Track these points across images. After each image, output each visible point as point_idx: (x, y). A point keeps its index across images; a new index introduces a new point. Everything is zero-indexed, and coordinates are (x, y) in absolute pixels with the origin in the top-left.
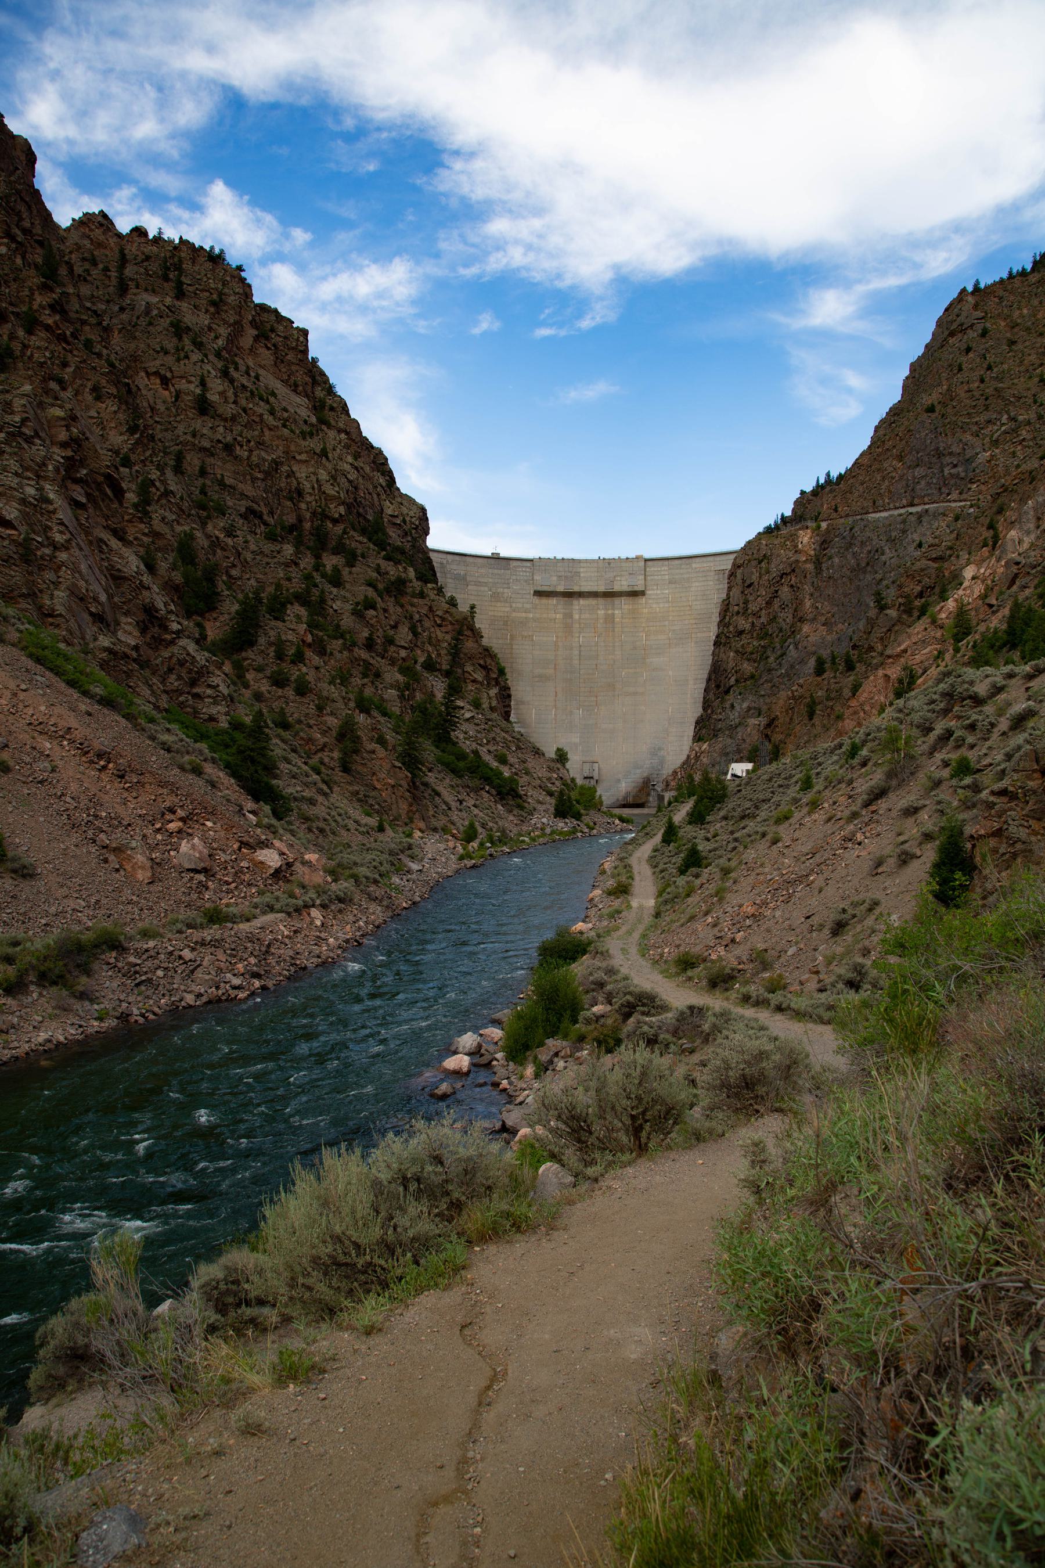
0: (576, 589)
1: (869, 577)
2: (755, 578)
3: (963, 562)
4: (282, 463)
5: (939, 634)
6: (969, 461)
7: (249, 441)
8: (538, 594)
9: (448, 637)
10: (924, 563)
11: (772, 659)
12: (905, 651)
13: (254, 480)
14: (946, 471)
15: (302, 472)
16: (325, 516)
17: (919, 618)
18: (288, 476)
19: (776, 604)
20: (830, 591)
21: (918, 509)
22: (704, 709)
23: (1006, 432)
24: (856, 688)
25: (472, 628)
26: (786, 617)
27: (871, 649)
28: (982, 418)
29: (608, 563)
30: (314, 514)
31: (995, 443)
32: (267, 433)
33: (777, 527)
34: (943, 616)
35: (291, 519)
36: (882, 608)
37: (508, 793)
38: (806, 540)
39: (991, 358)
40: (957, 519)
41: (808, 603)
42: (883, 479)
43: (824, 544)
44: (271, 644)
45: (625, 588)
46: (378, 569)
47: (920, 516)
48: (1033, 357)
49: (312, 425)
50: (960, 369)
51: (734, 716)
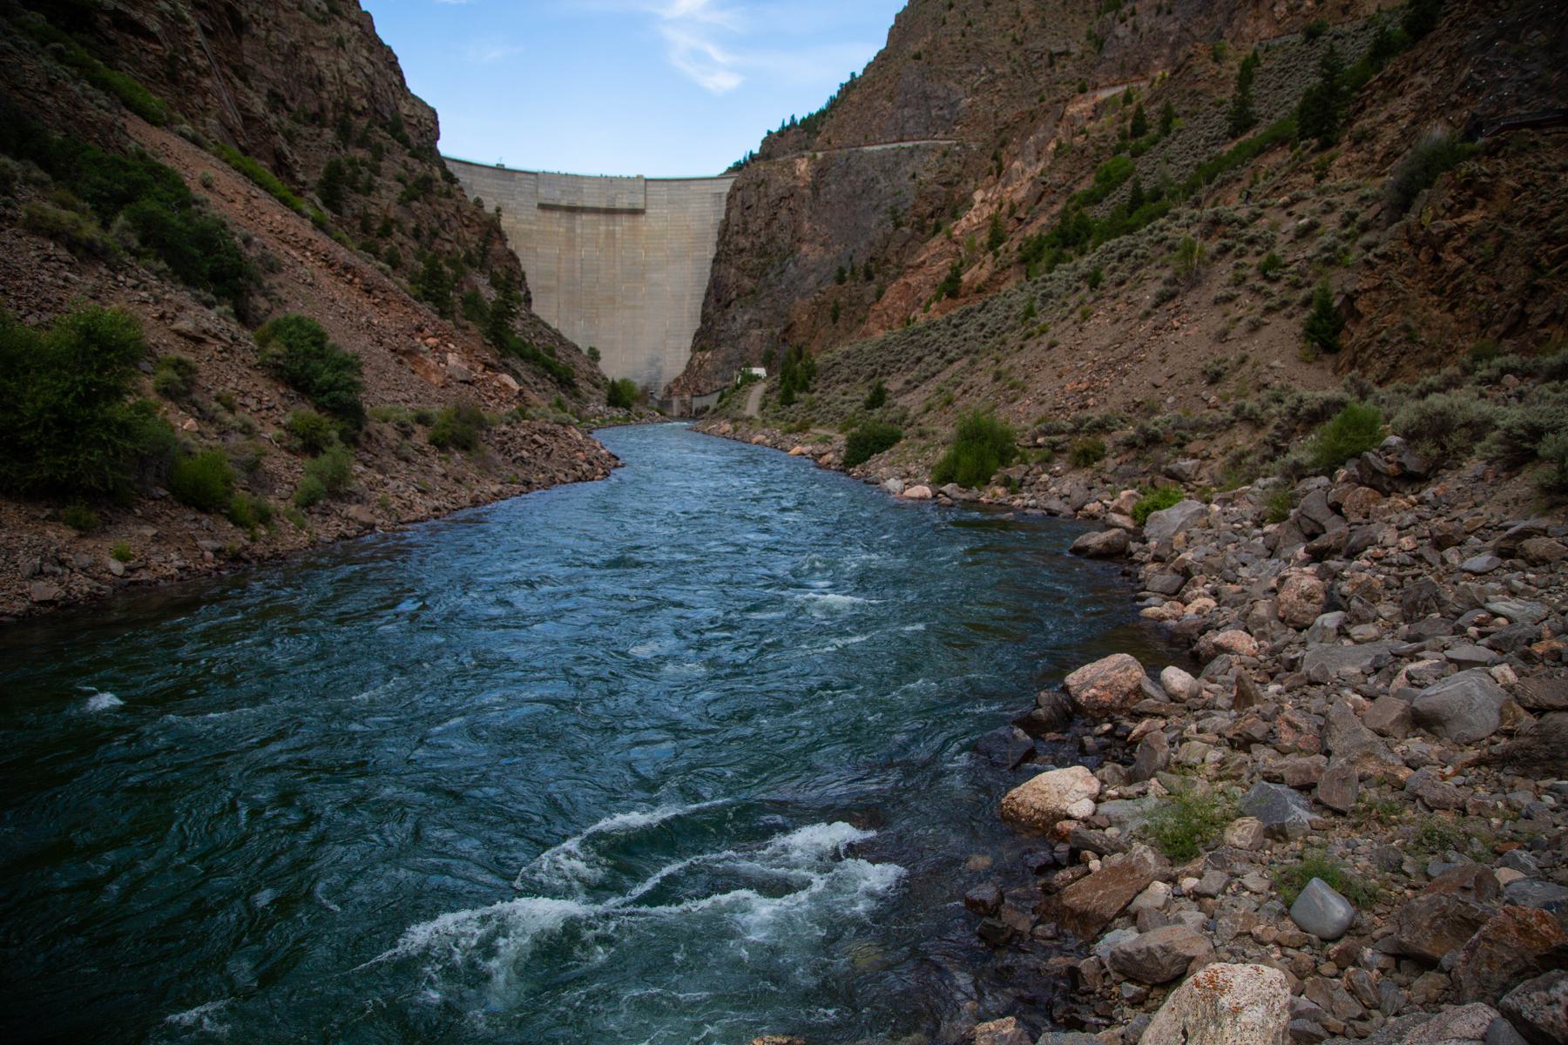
0: (579, 204)
1: (865, 204)
2: (754, 200)
3: (971, 187)
4: (301, 48)
5: (953, 248)
6: (954, 105)
7: (266, 20)
8: (543, 207)
9: (476, 238)
10: (936, 186)
11: (771, 276)
12: (924, 262)
13: (274, 62)
14: (934, 113)
15: (321, 60)
16: (348, 108)
17: (934, 234)
18: (308, 62)
19: (775, 225)
20: (827, 215)
21: (910, 144)
22: (704, 321)
23: (984, 83)
24: (879, 295)
25: (499, 231)
26: (785, 238)
27: (887, 261)
28: (964, 68)
29: (611, 180)
30: (336, 104)
31: (976, 91)
32: (282, 14)
33: (746, 163)
34: (957, 232)
35: (313, 107)
36: (898, 225)
37: (565, 382)
38: (803, 167)
39: (970, 15)
40: (945, 155)
41: (807, 225)
42: (874, 116)
43: (821, 171)
44: (355, 217)
45: (626, 206)
46: (405, 165)
47: (911, 151)
48: (1006, 19)
49: (323, 13)
50: (944, 23)
51: (736, 327)
